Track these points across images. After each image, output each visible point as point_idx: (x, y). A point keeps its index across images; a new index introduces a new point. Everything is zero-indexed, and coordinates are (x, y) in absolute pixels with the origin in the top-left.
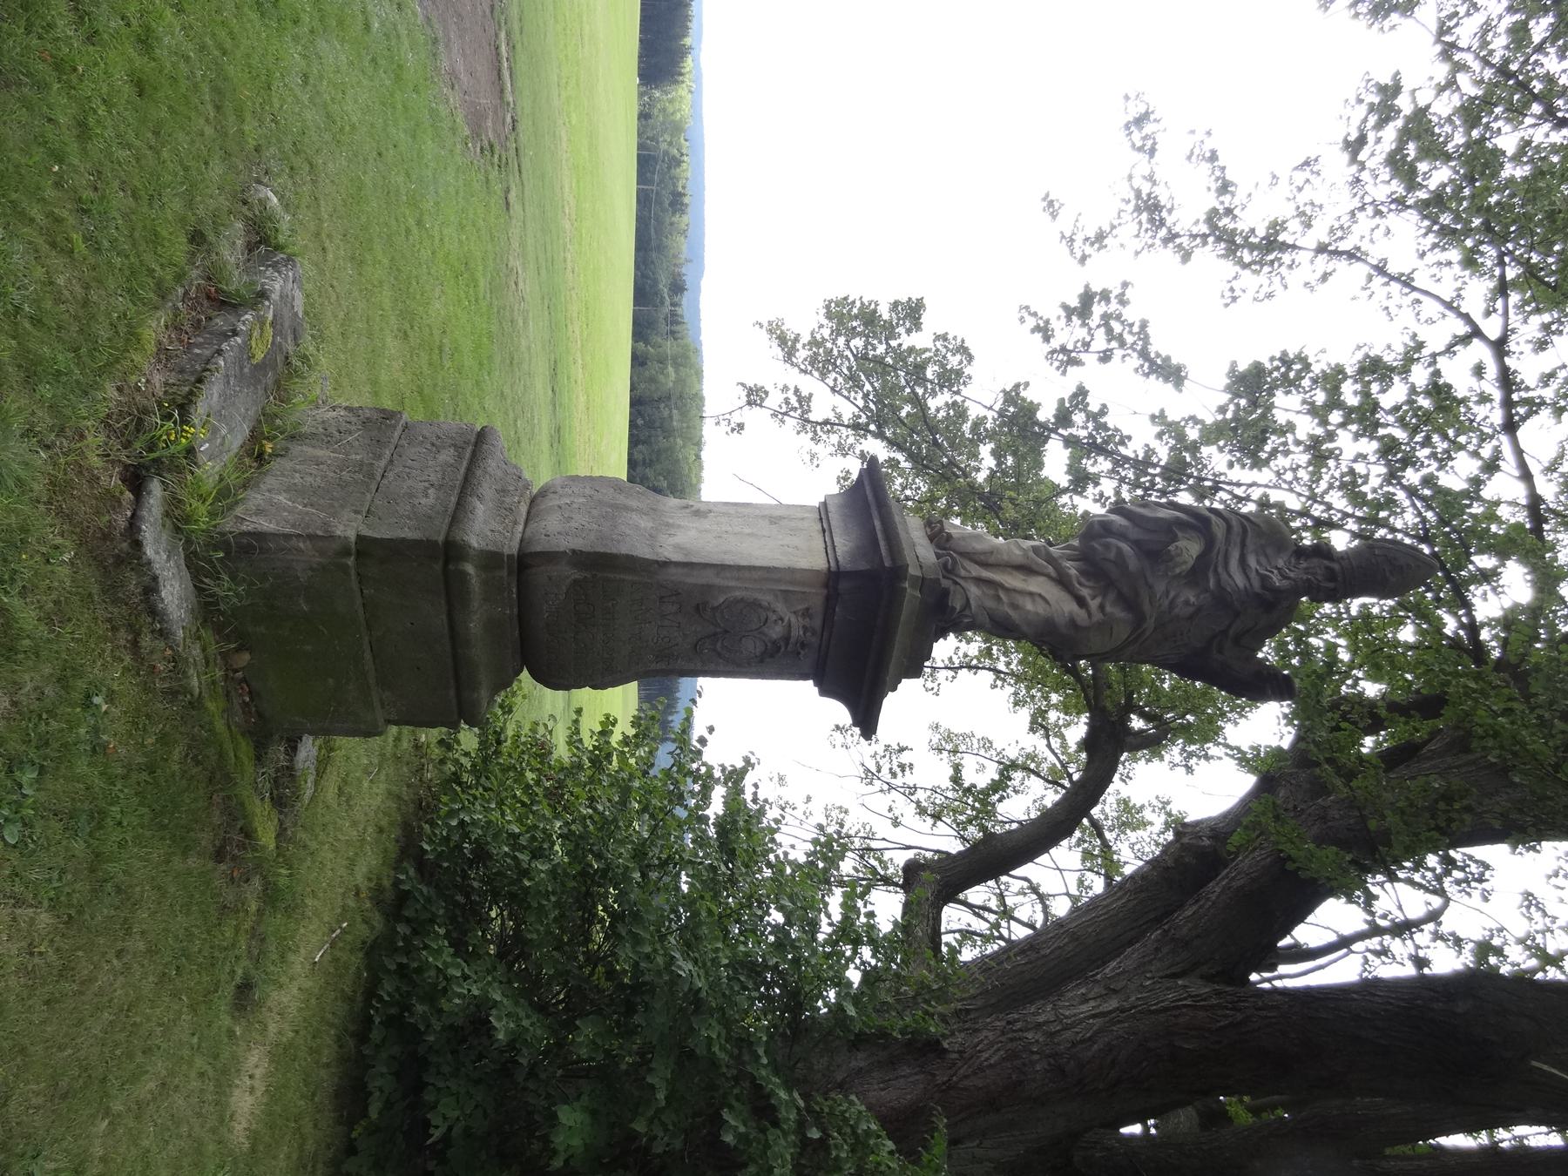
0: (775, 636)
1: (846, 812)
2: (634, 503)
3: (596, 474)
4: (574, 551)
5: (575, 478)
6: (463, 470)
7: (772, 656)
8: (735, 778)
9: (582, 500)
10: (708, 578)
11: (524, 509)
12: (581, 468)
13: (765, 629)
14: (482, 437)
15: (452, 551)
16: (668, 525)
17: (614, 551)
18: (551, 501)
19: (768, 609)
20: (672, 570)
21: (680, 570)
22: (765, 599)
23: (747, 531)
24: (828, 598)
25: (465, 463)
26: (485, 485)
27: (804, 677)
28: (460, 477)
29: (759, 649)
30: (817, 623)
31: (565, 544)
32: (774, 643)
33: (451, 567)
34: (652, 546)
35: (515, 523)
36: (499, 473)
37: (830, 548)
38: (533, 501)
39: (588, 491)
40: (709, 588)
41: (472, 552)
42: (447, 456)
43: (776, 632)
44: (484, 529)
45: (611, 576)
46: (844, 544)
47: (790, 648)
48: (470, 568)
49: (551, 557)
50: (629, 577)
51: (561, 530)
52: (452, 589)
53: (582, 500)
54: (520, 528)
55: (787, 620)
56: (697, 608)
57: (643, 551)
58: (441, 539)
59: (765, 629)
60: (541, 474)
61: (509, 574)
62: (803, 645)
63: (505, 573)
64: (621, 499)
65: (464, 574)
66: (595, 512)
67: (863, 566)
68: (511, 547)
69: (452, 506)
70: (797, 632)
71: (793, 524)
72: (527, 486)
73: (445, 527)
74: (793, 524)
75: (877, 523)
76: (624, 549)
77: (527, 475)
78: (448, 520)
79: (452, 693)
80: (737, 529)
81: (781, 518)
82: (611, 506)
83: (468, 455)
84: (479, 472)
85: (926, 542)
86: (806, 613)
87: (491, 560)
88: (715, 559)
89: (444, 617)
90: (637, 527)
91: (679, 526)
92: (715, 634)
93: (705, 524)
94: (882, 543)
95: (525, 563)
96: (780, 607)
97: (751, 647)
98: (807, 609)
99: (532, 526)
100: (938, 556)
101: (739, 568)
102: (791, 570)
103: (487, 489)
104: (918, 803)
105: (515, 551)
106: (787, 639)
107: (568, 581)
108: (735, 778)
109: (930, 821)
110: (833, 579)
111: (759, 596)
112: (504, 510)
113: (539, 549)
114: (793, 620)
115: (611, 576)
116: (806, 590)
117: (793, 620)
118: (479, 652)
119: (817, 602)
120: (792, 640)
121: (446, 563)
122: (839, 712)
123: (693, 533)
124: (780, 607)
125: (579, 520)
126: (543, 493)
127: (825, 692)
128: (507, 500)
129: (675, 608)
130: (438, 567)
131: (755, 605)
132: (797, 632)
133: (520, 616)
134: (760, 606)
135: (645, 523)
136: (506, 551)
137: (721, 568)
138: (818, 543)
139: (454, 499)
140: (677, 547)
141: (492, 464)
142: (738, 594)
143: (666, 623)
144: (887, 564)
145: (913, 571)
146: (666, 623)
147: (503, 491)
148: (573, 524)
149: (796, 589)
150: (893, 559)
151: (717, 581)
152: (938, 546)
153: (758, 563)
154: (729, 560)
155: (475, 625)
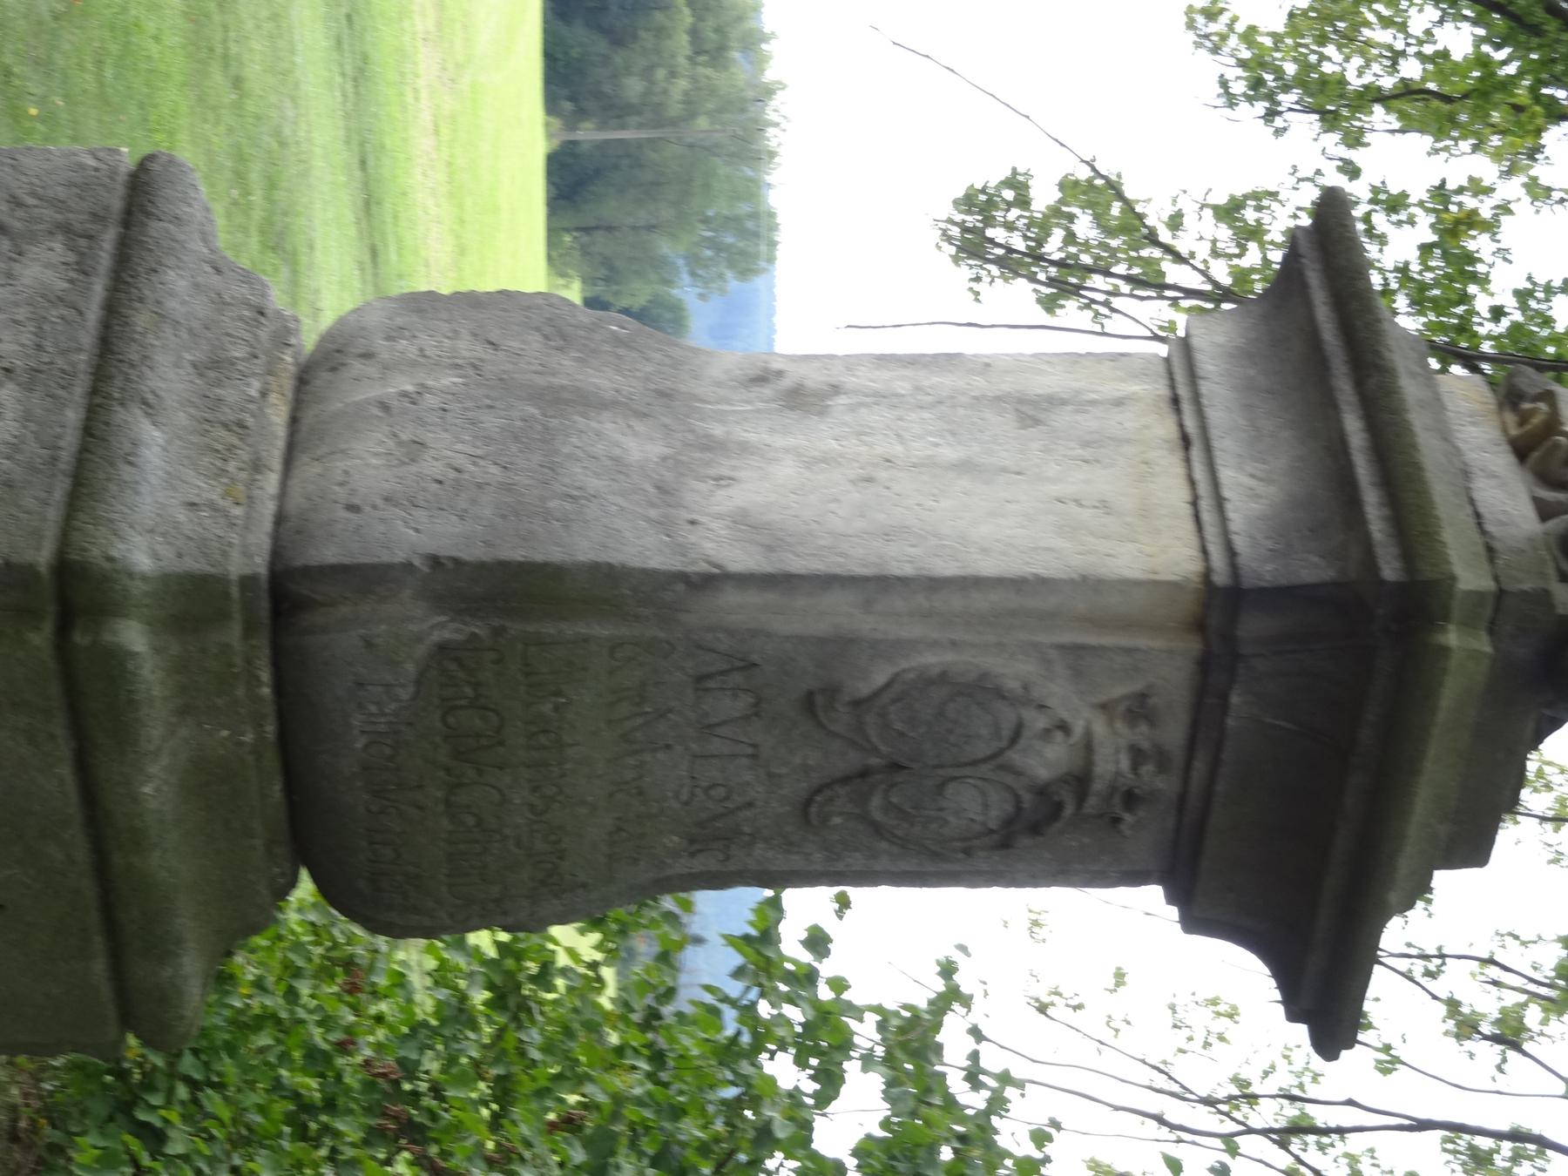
0: (1043, 773)
1: (1232, 1015)
2: (602, 380)
3: (488, 285)
4: (435, 561)
5: (424, 304)
6: (93, 314)
7: (1035, 829)
8: (911, 1040)
9: (450, 380)
10: (837, 614)
11: (278, 415)
12: (435, 264)
13: (1014, 757)
14: (142, 193)
15: (75, 593)
16: (711, 446)
17: (553, 553)
18: (361, 388)
19: (1025, 699)
20: (730, 598)
21: (753, 598)
22: (1013, 670)
23: (949, 453)
24: (1205, 664)
25: (99, 288)
26: (162, 359)
27: (1135, 878)
28: (88, 338)
29: (999, 809)
30: (1173, 734)
31: (413, 536)
32: (1042, 791)
33: (80, 638)
34: (665, 525)
35: (257, 466)
36: (201, 307)
37: (1206, 502)
38: (303, 377)
39: (467, 348)
40: (842, 646)
41: (137, 588)
42: (43, 267)
43: (1046, 760)
44: (173, 509)
45: (549, 629)
46: (1252, 489)
47: (1092, 803)
48: (133, 636)
49: (367, 579)
50: (602, 631)
51: (400, 492)
52: (88, 703)
53: (450, 380)
54: (272, 482)
55: (1076, 726)
56: (809, 704)
57: (641, 547)
58: (43, 556)
59: (1014, 757)
60: (328, 292)
61: (249, 630)
62: (1131, 799)
63: (233, 633)
64: (568, 370)
65: (115, 662)
66: (491, 422)
67: (1312, 569)
68: (248, 555)
69: (70, 441)
70: (1111, 763)
71: (1088, 422)
72: (284, 335)
73: (54, 514)
74: (1088, 422)
75: (1353, 425)
76: (582, 547)
77: (277, 298)
78: (61, 487)
79: (100, 967)
80: (920, 449)
81: (1054, 402)
82: (539, 396)
83: (104, 259)
84: (141, 320)
85: (1501, 461)
86: (1139, 709)
87: (192, 602)
88: (858, 558)
89: (66, 771)
90: (619, 465)
91: (745, 448)
92: (864, 773)
93: (822, 435)
94: (1371, 498)
95: (290, 599)
96: (1061, 696)
97: (973, 805)
98: (1142, 697)
99: (308, 470)
100: (1545, 511)
101: (934, 584)
102: (1089, 584)
103: (168, 373)
104: (1453, 1005)
105: (260, 565)
106: (1080, 781)
107: (421, 650)
108: (911, 1040)
109: (1489, 1053)
110: (1220, 611)
111: (993, 663)
112: (222, 429)
113: (330, 554)
114: (1100, 728)
115: (549, 629)
116: (1142, 642)
117: (1100, 728)
118: (171, 859)
119: (1170, 668)
120: (1098, 786)
121: (65, 623)
122: (1241, 975)
123: (786, 471)
124: (1061, 696)
125: (448, 450)
126: (336, 352)
127: (1196, 920)
128: (229, 394)
129: (744, 703)
130: (41, 638)
131: (983, 690)
132: (1111, 763)
133: (285, 739)
134: (1000, 694)
135: (641, 446)
136: (236, 567)
137: (880, 585)
138: (1170, 490)
139: (73, 416)
140: (742, 521)
141: (177, 289)
142: (931, 660)
143: (716, 746)
144: (1390, 570)
145: (1470, 577)
146: (716, 746)
147: (215, 367)
148: (431, 467)
149: (1108, 640)
150: (1408, 555)
151: (867, 625)
152: (1544, 477)
153: (988, 567)
154: (901, 559)
155: (155, 785)
